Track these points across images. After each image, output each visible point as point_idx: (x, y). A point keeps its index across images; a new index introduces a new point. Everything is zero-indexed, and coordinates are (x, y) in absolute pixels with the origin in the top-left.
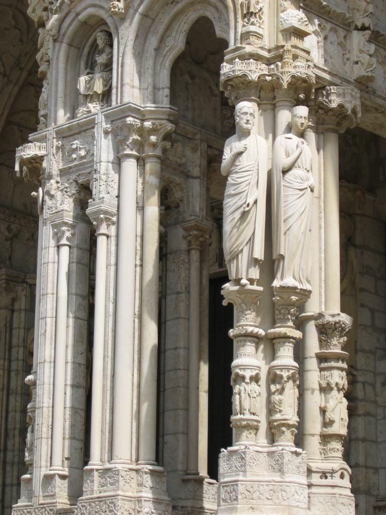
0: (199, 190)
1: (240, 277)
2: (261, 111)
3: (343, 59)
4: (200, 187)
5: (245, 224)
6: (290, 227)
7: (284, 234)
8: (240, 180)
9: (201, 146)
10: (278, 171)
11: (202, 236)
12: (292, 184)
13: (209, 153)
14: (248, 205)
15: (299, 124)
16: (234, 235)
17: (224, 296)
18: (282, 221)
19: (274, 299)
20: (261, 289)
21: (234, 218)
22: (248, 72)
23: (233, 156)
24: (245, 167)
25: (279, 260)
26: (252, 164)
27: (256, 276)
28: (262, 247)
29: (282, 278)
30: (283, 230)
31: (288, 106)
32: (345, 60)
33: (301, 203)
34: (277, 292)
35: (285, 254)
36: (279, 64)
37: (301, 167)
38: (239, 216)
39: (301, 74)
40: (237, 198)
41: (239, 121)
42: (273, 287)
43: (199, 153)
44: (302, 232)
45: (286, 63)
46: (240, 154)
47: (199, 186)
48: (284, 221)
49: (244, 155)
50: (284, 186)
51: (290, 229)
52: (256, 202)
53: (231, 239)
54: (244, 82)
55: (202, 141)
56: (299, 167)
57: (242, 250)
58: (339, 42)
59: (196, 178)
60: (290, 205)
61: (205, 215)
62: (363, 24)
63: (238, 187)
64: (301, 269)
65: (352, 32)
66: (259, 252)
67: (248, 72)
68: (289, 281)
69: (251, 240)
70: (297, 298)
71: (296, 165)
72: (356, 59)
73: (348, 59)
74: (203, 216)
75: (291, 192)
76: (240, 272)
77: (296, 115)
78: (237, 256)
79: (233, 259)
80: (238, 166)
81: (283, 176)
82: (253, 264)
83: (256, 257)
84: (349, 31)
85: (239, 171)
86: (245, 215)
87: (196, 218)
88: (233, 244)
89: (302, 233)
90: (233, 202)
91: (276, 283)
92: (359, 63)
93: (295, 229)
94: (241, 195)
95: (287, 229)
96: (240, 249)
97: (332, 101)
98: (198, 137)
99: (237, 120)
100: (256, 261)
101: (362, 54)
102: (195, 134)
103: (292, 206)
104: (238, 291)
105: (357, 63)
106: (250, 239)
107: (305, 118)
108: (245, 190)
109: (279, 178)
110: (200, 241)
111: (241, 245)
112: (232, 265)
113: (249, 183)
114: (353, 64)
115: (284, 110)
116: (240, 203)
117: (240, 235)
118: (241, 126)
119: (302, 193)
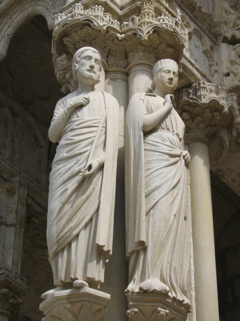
0: (13, 239)
1: (73, 277)
2: (108, 80)
3: (210, 71)
4: (15, 237)
5: (84, 197)
6: (156, 203)
7: (146, 215)
8: (77, 138)
9: (19, 190)
10: (137, 130)
11: (13, 297)
12: (158, 146)
13: (29, 201)
14: (90, 167)
15: (166, 80)
16: (65, 214)
17: (44, 313)
18: (143, 195)
19: (129, 311)
20: (108, 296)
21: (67, 189)
22: (93, 17)
23: (69, 109)
24: (85, 122)
25: (137, 253)
26: (98, 119)
27: (99, 276)
28: (109, 236)
29: (142, 279)
30: (144, 210)
31: (147, 71)
32: (213, 72)
33: (172, 174)
34: (133, 300)
35: (147, 239)
36: (137, 19)
37: (171, 130)
38: (75, 185)
39: (167, 26)
40: (73, 161)
41: (79, 68)
42: (128, 291)
43: (16, 197)
44: (174, 213)
45: (146, 14)
46: (80, 107)
47: (13, 236)
48: (146, 196)
49: (85, 109)
50: (145, 150)
51: (156, 207)
52: (101, 167)
53: (60, 219)
54: (86, 39)
55: (20, 185)
56: (168, 129)
57: (77, 235)
58: (205, 50)
59: (11, 226)
60: (155, 174)
61: (19, 272)
62: (234, 36)
63: (76, 147)
64: (173, 269)
65: (219, 45)
66: (105, 237)
67: (93, 17)
68: (154, 283)
69: (93, 221)
70: (167, 300)
71: (163, 125)
72: (225, 71)
73: (216, 71)
74: (16, 274)
75: (156, 156)
76: (73, 270)
77: (161, 69)
78: (70, 245)
79: (63, 249)
80: (74, 121)
81: (144, 139)
82: (95, 256)
83: (101, 243)
84: (215, 44)
85: (76, 127)
86: (85, 181)
87: (7, 272)
88: (64, 227)
89: (174, 216)
90: (66, 167)
91: (133, 287)
92: (231, 75)
93: (163, 206)
94: (79, 157)
95: (150, 207)
96: (75, 233)
97: (202, 96)
98: (17, 179)
99: (75, 66)
100: (100, 252)
101: (233, 65)
102: (13, 175)
103: (158, 175)
104: (68, 297)
105: (228, 75)
106: (91, 220)
107: (174, 73)
108: (87, 151)
109: (137, 139)
110: (10, 303)
111: (75, 229)
112: (60, 259)
113: (92, 143)
114: (223, 76)
115: (143, 74)
116: (76, 169)
117: (75, 214)
118: (82, 76)
119: (173, 160)
